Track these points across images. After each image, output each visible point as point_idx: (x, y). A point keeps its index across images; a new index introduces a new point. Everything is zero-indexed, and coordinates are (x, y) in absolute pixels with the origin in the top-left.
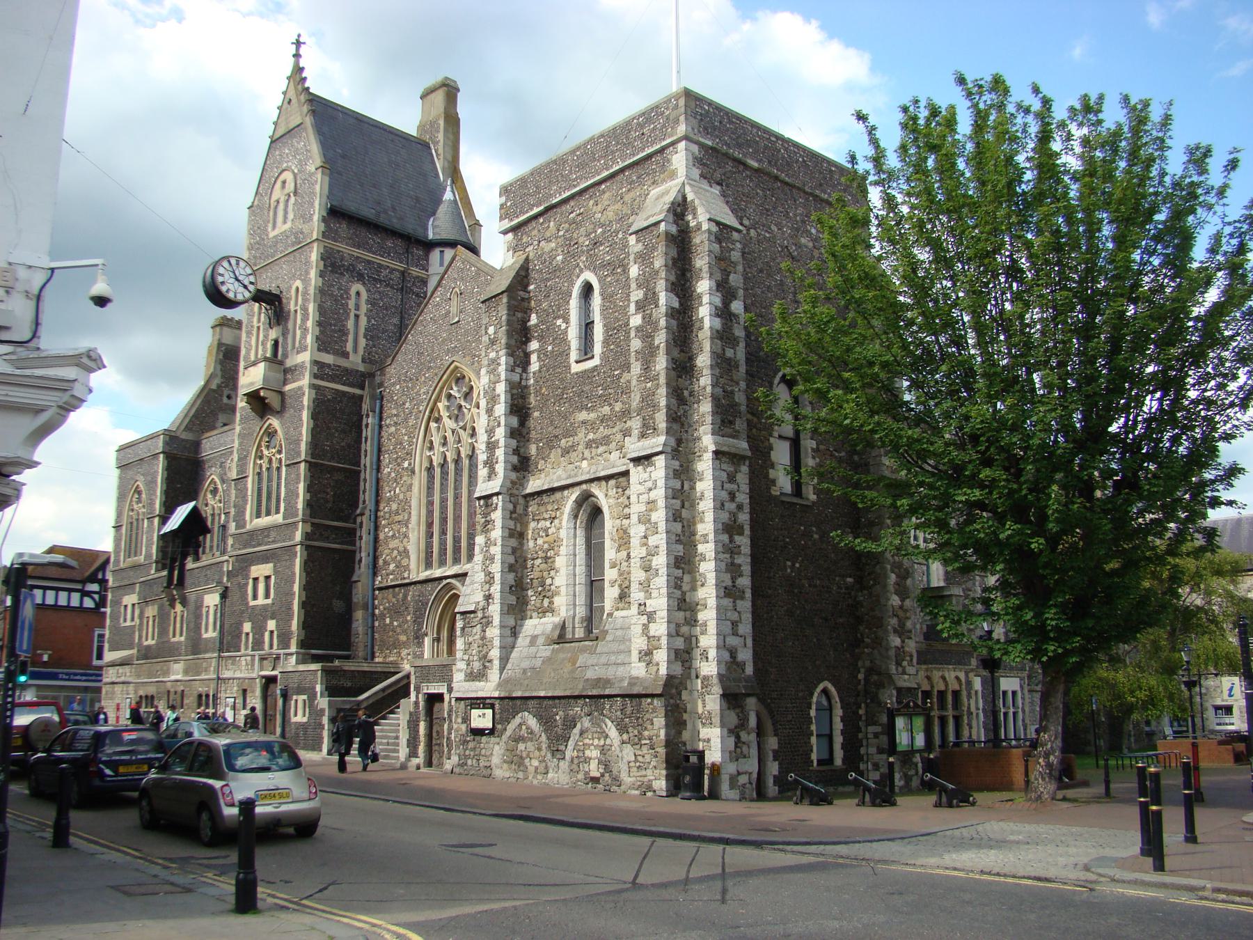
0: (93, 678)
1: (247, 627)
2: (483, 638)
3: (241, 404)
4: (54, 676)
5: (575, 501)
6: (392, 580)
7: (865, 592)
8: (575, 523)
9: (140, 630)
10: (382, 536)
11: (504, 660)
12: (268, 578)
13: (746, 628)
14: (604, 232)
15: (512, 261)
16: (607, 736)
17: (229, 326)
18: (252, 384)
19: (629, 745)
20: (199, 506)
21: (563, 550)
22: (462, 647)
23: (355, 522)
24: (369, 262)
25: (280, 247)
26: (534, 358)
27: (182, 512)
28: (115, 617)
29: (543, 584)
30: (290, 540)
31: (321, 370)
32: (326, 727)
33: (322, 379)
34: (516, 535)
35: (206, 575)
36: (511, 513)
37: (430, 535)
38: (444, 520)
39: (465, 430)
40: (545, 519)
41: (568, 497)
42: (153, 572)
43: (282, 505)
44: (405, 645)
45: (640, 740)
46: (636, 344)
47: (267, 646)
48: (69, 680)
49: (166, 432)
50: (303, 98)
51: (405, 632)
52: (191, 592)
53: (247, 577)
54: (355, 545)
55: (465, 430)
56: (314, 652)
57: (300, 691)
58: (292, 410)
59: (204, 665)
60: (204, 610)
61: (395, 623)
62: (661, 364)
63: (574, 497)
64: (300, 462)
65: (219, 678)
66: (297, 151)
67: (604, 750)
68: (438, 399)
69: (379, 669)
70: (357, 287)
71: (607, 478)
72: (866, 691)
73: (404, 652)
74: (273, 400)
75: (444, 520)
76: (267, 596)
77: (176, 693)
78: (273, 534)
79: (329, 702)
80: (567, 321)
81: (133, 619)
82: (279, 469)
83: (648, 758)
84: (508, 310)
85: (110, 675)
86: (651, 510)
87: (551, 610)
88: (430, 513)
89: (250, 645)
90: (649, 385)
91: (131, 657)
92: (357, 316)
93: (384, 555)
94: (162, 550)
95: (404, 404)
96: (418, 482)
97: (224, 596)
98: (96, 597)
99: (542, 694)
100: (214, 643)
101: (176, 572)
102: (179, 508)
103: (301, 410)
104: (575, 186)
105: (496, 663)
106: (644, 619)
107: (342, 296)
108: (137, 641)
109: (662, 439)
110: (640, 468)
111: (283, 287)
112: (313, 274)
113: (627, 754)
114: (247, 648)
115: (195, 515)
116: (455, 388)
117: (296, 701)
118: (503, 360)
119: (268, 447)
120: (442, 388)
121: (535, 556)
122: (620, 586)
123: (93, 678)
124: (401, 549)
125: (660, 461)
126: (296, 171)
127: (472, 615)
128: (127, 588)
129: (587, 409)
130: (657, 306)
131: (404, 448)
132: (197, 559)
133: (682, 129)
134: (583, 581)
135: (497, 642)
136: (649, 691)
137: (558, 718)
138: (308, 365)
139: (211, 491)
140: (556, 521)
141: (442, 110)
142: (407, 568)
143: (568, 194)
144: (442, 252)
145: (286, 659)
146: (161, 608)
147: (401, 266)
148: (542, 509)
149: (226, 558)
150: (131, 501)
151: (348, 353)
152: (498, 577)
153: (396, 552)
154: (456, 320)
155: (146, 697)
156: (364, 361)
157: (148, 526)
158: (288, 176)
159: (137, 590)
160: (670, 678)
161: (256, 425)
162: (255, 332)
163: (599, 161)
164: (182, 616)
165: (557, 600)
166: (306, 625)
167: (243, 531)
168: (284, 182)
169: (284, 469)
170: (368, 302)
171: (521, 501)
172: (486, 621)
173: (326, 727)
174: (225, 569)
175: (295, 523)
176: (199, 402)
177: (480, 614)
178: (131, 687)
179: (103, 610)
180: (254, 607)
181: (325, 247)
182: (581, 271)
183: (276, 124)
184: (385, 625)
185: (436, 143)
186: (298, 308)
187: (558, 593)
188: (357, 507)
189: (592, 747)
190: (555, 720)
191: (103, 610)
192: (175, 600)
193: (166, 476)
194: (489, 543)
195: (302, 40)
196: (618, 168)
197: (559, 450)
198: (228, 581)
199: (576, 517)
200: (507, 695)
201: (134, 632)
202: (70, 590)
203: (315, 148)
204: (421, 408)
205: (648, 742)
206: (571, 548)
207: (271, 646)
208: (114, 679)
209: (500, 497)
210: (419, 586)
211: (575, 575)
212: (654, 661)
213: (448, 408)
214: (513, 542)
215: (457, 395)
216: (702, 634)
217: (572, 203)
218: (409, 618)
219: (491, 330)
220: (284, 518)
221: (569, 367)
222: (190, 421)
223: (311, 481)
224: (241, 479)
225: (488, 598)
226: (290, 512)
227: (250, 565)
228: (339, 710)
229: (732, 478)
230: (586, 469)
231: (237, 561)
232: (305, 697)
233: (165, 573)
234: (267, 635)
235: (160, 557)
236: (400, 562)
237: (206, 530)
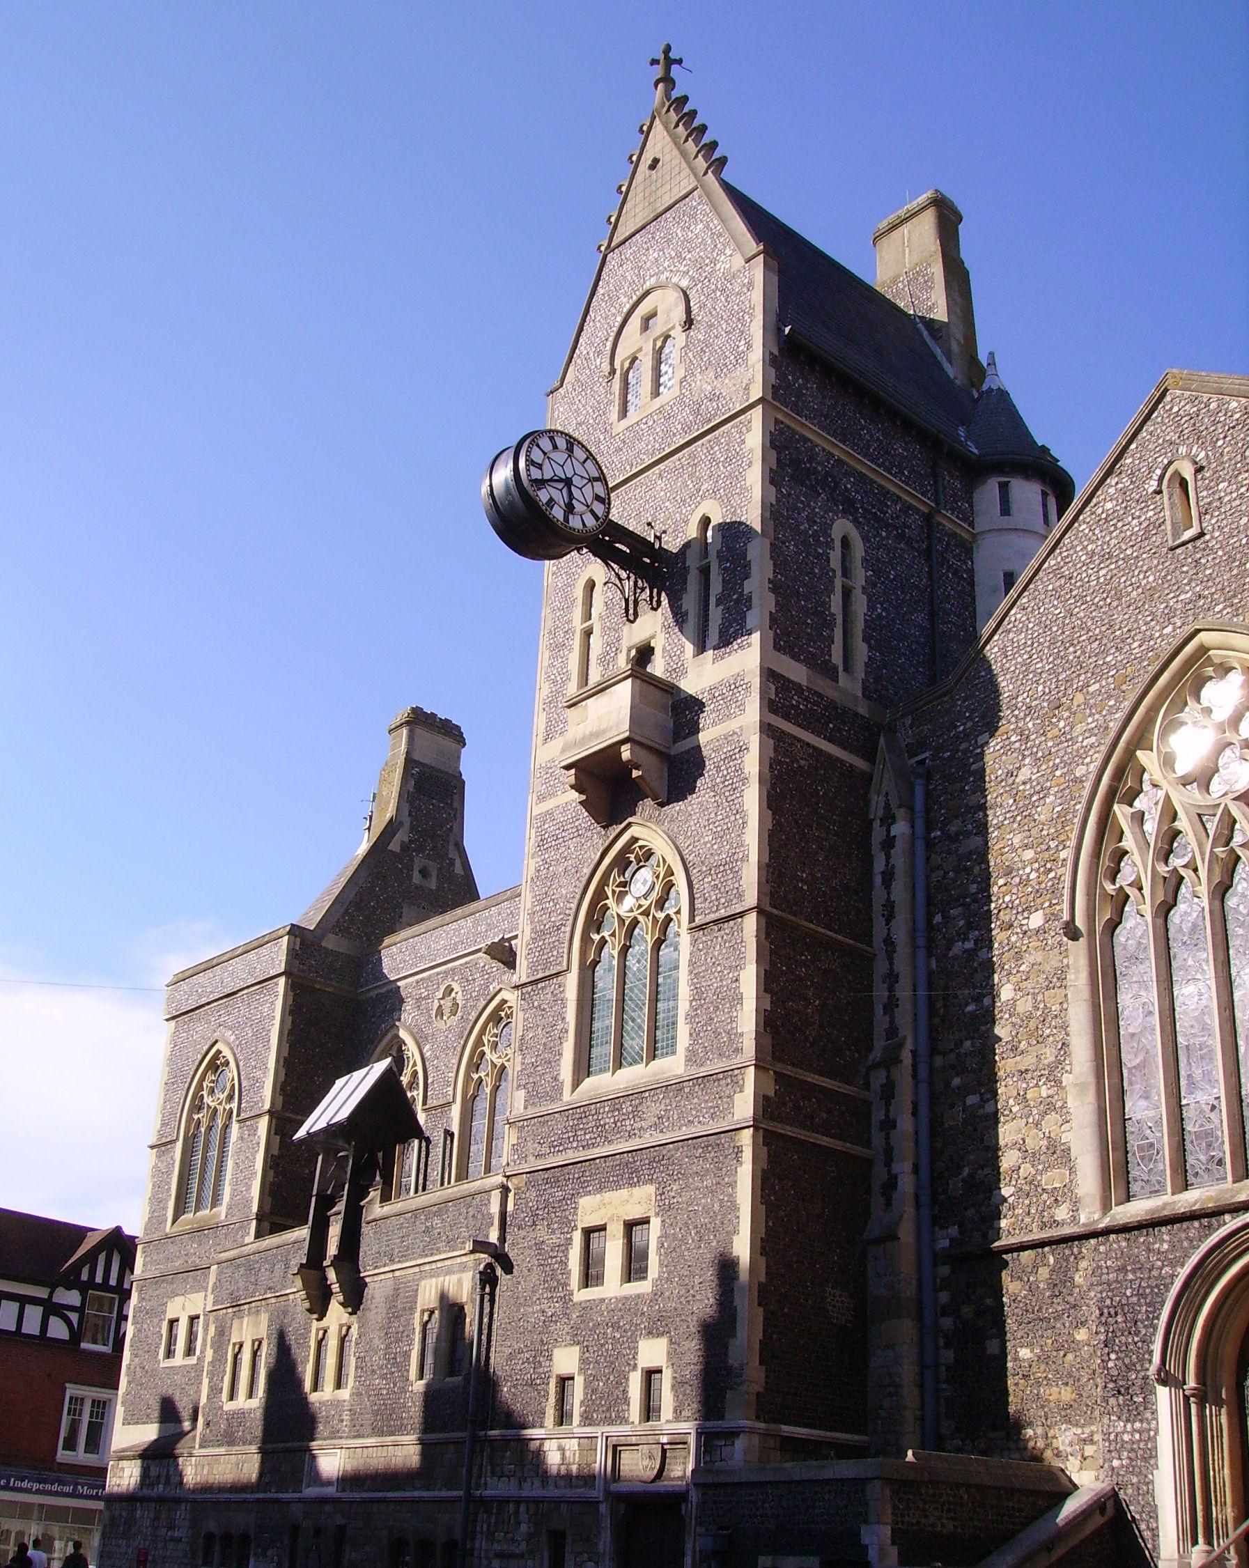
1: (566, 1360)
18: (596, 735)
33: (786, 717)
35: (427, 1231)
51: (1069, 1378)
54: (868, 1144)
64: (741, 914)
70: (842, 527)
77: (318, 1531)
92: (847, 593)
98: (74, 1317)
102: (339, 1083)
138: (756, 682)
142: (1065, 1193)
144: (1004, 487)
147: (923, 503)
155: (227, 1537)
159: (212, 1279)
180: (588, 1306)
181: (777, 422)
188: (870, 1049)
193: (288, 1026)
218: (1081, 1335)
223: (772, 964)
235: (267, 1208)
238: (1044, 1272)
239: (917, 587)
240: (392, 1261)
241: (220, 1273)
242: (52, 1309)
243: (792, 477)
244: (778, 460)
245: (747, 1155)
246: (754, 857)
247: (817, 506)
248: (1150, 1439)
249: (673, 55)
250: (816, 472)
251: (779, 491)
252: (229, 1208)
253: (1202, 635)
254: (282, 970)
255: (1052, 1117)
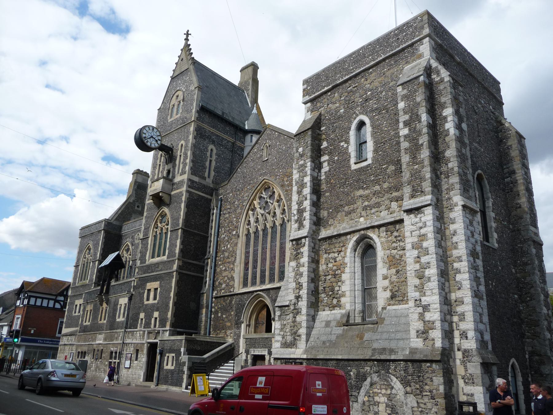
0: (55, 343)
1: (142, 315)
2: (294, 322)
3: (149, 201)
4: (36, 341)
5: (356, 241)
6: (223, 293)
7: (524, 304)
8: (355, 254)
9: (83, 317)
10: (218, 270)
11: (308, 335)
12: (156, 289)
13: (486, 319)
14: (371, 94)
15: (310, 117)
16: (392, 388)
17: (141, 174)
18: (156, 190)
19: (412, 396)
20: (120, 253)
21: (347, 270)
22: (279, 327)
23: (204, 262)
24: (217, 136)
25: (174, 126)
26: (325, 164)
27: (111, 257)
28: (70, 311)
29: (333, 290)
30: (170, 269)
31: (191, 184)
32: (186, 373)
33: (192, 188)
34: (315, 261)
36: (313, 249)
37: (246, 269)
38: (255, 261)
39: (269, 214)
40: (334, 252)
41: (350, 239)
42: (92, 288)
43: (167, 251)
44: (230, 328)
45: (421, 392)
46: (405, 145)
47: (152, 326)
48: (43, 343)
49: (105, 220)
50: (190, 62)
51: (230, 321)
52: (112, 297)
53: (144, 289)
54: (203, 274)
55: (269, 214)
56: (178, 330)
57: (171, 351)
58: (176, 204)
59: (116, 335)
60: (119, 306)
61: (224, 316)
62: (425, 154)
63: (355, 238)
64: (179, 229)
65: (123, 343)
66: (185, 81)
67: (390, 397)
68: (254, 199)
69: (215, 341)
70: (211, 147)
71: (379, 227)
72: (530, 366)
73: (229, 332)
74: (166, 198)
75: (255, 261)
76: (155, 298)
77: (98, 350)
78: (161, 267)
79: (189, 358)
80: (347, 142)
81: (79, 312)
82: (166, 233)
83: (429, 405)
84: (312, 138)
85: (64, 341)
86: (422, 240)
87: (339, 305)
88: (247, 257)
89: (143, 325)
90: (416, 167)
91: (76, 331)
92: (211, 161)
93: (220, 280)
94: (99, 277)
95: (234, 203)
96: (242, 242)
97: (130, 299)
98: (62, 303)
99: (340, 357)
100: (123, 324)
101: (105, 287)
102: (110, 255)
103: (180, 203)
104: (352, 73)
105: (304, 337)
106: (420, 310)
107: (204, 150)
108: (80, 323)
109: (429, 197)
110: (412, 216)
111: (174, 144)
112: (191, 137)
113: (411, 402)
114: (141, 327)
115: (118, 257)
116: (264, 193)
117: (168, 357)
118: (309, 164)
119: (161, 223)
120: (257, 193)
121: (327, 274)
122: (391, 290)
123: (55, 343)
124: (230, 276)
125: (429, 211)
126: (184, 90)
127: (287, 308)
128: (79, 296)
129: (363, 188)
130: (420, 122)
131: (234, 224)
132: (117, 279)
133: (426, 31)
134: (360, 288)
135: (304, 324)
136: (430, 358)
137: (352, 373)
139: (126, 250)
140: (342, 253)
141: (251, 76)
142: (233, 286)
143: (347, 77)
144: (252, 136)
145: (163, 333)
146: (95, 306)
147: (232, 140)
148: (332, 247)
149: (134, 279)
150: (85, 253)
151: (206, 178)
152: (305, 285)
153: (226, 278)
154: (266, 159)
155: (82, 352)
156: (213, 182)
157: (92, 265)
158: (180, 93)
160: (444, 349)
161: (156, 213)
162: (158, 167)
163: (368, 57)
164: (106, 310)
165: (343, 300)
166: (175, 315)
167: (144, 265)
168: (177, 96)
169: (169, 233)
170: (216, 154)
171: (318, 242)
172: (297, 312)
173: (186, 373)
174: (132, 285)
175: (174, 261)
176: (123, 207)
177: (292, 307)
178: (74, 348)
179: (64, 309)
180: (147, 305)
181: (197, 125)
182: (357, 115)
183: (174, 71)
184: (218, 317)
185: (248, 90)
186: (182, 154)
187: (343, 295)
188: (206, 255)
189: (380, 395)
190: (350, 375)
191: (64, 309)
192: (103, 301)
193: (104, 241)
194: (299, 265)
195: (189, 33)
196: (381, 58)
197: (344, 213)
198: (133, 291)
199: (355, 251)
200: (312, 357)
201: (79, 319)
202: (49, 299)
203: (195, 79)
204: (244, 204)
205: (429, 394)
206: (353, 268)
207: (155, 326)
208: (66, 343)
209: (307, 239)
210: (240, 296)
211: (355, 285)
212: (430, 338)
213: (259, 204)
214: (314, 265)
215: (265, 197)
216: (460, 320)
217: (350, 82)
218: (232, 313)
219: (301, 150)
220: (168, 258)
221: (350, 167)
222: (118, 216)
224: (145, 239)
225: (298, 297)
226: (171, 254)
227: (147, 283)
228: (193, 363)
229: (471, 223)
230: (363, 222)
231: (139, 280)
232: (174, 355)
233: (99, 288)
234: (153, 320)
235: (97, 281)
236: (228, 283)
237: (122, 266)
238: (228, 301)
239: (228, 159)
240: (115, 294)
241: (85, 295)
242: (56, 301)
243: (200, 137)
244: (197, 133)
245: (174, 277)
246: (182, 217)
247: (205, 143)
248: (240, 333)
249: (189, 33)
250: (206, 135)
251: (196, 140)
252: (89, 281)
253: (265, 180)
254: (103, 228)
255: (233, 271)
